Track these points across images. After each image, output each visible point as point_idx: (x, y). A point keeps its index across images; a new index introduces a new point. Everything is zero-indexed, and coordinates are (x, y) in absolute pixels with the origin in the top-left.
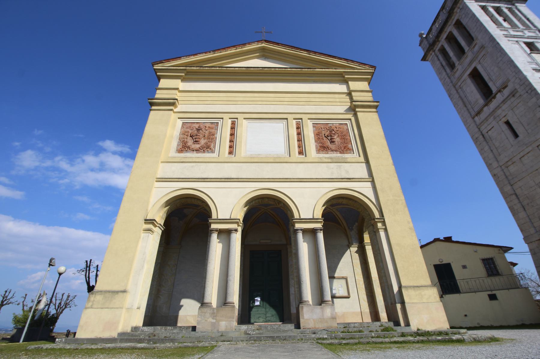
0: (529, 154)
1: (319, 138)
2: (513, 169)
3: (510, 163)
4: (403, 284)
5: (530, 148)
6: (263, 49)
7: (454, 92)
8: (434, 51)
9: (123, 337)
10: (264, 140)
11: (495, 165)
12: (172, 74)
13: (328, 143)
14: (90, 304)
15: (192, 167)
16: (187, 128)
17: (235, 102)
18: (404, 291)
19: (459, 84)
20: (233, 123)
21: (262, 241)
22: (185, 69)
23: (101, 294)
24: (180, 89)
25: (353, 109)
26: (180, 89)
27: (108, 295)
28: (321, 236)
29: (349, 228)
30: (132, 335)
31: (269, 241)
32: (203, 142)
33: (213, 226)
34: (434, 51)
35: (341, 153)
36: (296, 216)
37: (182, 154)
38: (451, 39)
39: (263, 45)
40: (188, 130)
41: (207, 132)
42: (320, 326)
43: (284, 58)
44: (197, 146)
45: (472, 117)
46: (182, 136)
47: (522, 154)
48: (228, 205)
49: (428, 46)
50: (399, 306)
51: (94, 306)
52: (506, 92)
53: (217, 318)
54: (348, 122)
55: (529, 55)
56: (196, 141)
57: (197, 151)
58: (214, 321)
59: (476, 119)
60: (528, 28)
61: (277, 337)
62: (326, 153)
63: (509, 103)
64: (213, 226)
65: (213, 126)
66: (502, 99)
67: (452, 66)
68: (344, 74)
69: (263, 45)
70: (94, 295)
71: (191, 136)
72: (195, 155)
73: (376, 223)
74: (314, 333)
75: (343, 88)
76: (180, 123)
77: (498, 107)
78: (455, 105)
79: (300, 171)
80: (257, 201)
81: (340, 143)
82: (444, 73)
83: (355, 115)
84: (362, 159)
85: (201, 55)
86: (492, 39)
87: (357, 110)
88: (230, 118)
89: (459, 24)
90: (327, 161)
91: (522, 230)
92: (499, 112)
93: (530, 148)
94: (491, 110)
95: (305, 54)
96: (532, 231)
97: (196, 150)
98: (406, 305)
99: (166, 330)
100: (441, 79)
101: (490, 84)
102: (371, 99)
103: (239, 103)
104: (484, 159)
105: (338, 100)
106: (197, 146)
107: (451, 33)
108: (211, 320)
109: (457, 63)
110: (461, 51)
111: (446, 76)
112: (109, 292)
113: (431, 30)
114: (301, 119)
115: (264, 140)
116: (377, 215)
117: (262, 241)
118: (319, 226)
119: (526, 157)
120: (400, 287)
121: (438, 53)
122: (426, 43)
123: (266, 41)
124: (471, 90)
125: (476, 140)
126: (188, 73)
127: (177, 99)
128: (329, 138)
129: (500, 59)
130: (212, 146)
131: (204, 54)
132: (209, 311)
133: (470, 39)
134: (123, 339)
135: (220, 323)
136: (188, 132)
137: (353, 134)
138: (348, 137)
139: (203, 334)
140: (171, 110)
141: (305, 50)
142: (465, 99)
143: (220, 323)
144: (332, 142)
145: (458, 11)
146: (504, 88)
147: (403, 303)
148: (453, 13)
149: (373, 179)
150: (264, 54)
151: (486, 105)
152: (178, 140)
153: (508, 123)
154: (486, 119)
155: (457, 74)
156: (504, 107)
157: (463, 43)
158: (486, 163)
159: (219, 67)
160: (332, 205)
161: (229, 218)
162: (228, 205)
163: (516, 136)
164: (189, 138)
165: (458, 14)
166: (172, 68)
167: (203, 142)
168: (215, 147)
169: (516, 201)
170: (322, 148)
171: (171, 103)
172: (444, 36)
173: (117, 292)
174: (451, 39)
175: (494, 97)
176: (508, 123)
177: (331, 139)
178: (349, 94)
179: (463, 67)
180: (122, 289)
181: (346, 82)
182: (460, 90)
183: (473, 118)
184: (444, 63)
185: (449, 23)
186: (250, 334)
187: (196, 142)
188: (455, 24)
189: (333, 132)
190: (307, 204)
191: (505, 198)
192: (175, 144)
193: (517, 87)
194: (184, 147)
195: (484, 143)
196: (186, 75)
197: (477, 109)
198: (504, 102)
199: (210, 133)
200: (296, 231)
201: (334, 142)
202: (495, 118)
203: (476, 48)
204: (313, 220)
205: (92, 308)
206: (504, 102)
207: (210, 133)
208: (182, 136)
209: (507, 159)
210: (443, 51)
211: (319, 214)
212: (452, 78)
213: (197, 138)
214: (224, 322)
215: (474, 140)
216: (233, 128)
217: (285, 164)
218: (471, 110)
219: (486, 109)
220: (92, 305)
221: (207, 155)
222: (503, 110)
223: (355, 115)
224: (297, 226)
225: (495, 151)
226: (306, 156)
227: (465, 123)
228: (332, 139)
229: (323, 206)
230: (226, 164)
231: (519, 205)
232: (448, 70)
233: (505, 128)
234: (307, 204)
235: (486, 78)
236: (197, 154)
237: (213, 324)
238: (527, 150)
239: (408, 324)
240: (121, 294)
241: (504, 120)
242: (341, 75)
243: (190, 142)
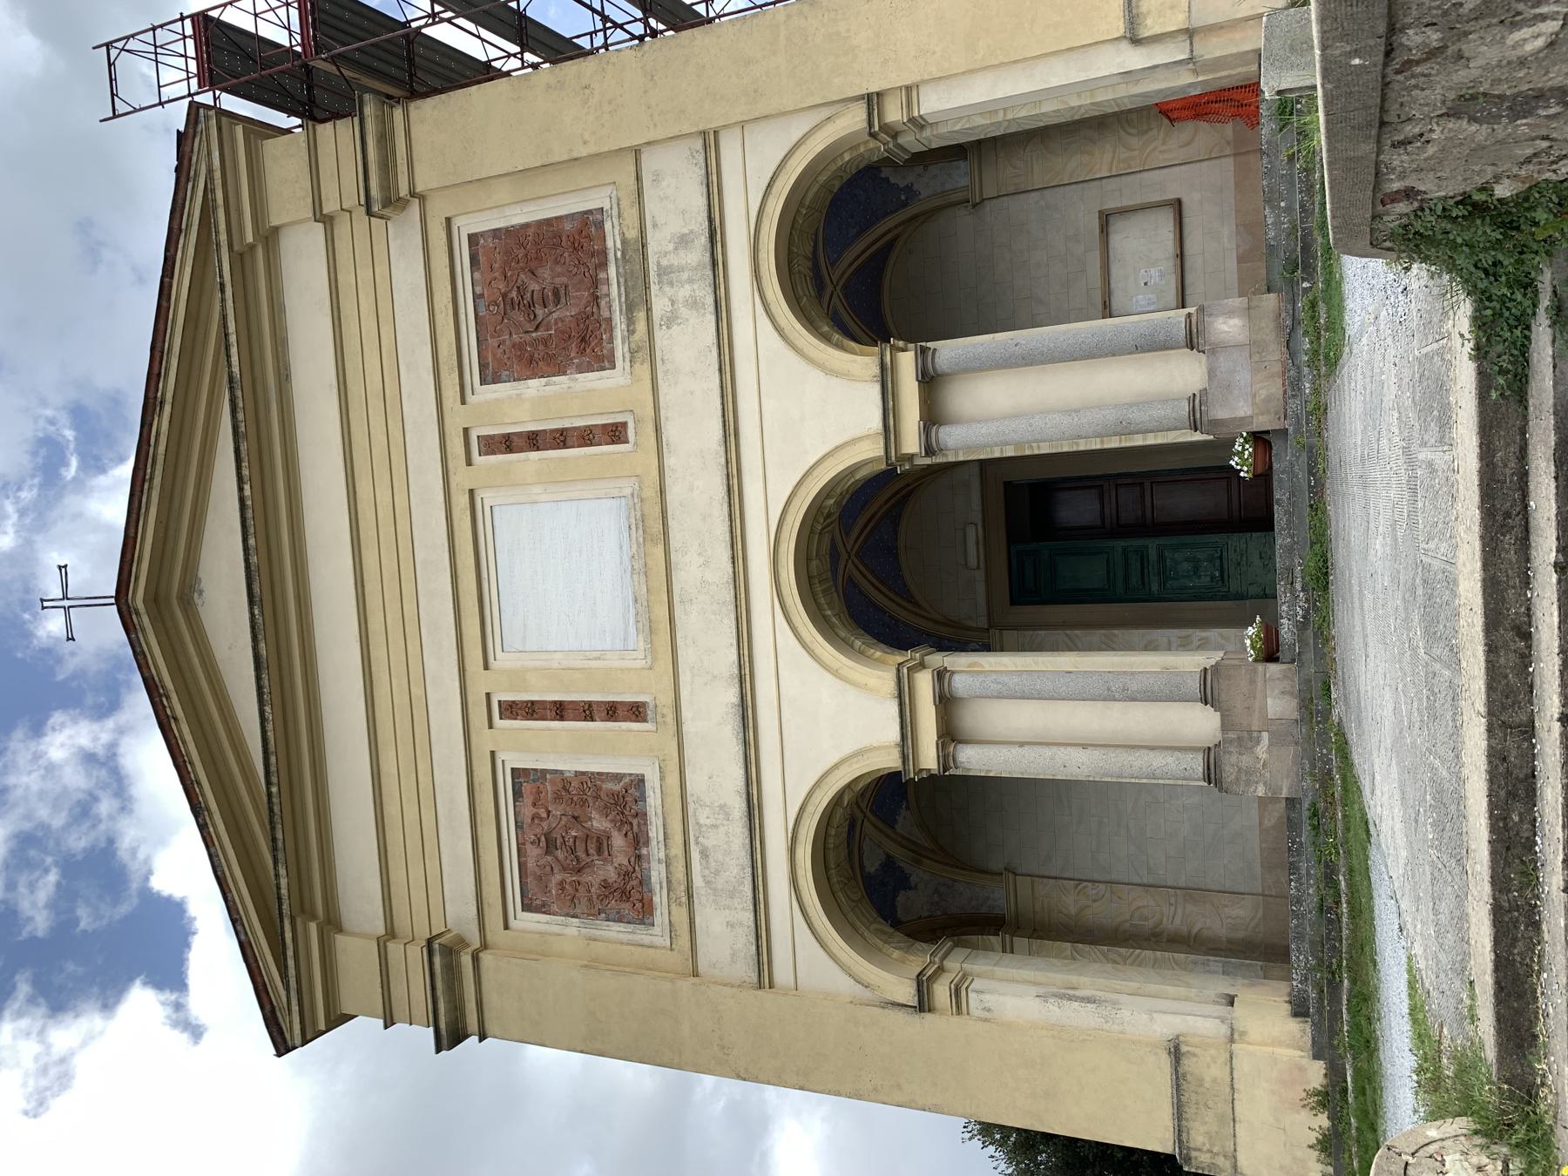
9: (1321, 1049)
10: (563, 577)
13: (565, 313)
14: (1220, 1161)
15: (704, 854)
16: (546, 890)
17: (417, 710)
20: (511, 710)
21: (973, 561)
24: (390, 945)
29: (905, 205)
31: (971, 534)
32: (599, 823)
33: (929, 759)
35: (603, 265)
42: (1277, 356)
44: (618, 841)
46: (582, 907)
48: (841, 715)
53: (1255, 728)
57: (638, 840)
58: (1265, 735)
62: (611, 329)
64: (929, 759)
65: (527, 788)
72: (656, 851)
80: (818, 588)
81: (559, 269)
90: (641, 326)
105: (365, 274)
106: (618, 841)
108: (1262, 751)
115: (563, 577)
117: (973, 561)
127: (430, 942)
132: (1234, 759)
136: (561, 884)
138: (530, 232)
140: (476, 959)
159: (273, 829)
160: (819, 285)
162: (841, 715)
164: (586, 878)
166: (292, 971)
167: (599, 823)
168: (617, 777)
170: (585, 345)
180: (1165, 1062)
186: (1307, 611)
187: (602, 844)
189: (514, 294)
190: (822, 411)
194: (628, 897)
196: (314, 917)
199: (558, 798)
204: (887, 381)
207: (558, 798)
208: (582, 907)
211: (862, 363)
216: (531, 710)
221: (653, 801)
228: (547, 296)
234: (822, 411)
236: (654, 843)
242: (241, 259)
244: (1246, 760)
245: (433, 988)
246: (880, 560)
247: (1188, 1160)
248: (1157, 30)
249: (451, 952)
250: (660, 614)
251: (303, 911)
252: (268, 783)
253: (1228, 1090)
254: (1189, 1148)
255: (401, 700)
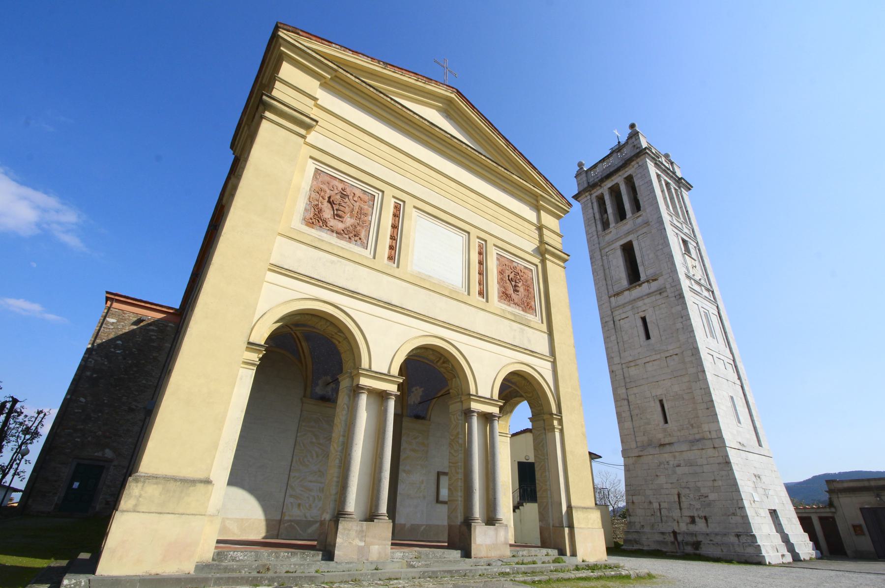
0: (655, 363)
1: (502, 279)
2: (633, 371)
3: (632, 364)
4: (573, 504)
5: (658, 356)
6: (449, 101)
7: (597, 254)
8: (591, 195)
11: (617, 360)
12: (312, 64)
15: (333, 262)
18: (576, 515)
19: (607, 250)
20: (397, 207)
22: (336, 71)
23: (156, 484)
25: (542, 251)
26: (318, 102)
27: (172, 485)
28: (391, 404)
30: (218, 568)
34: (591, 195)
35: (523, 310)
36: (365, 364)
37: (313, 230)
38: (615, 191)
39: (453, 96)
40: (325, 187)
41: (357, 205)
43: (473, 132)
45: (608, 296)
46: (314, 195)
47: (648, 359)
48: (383, 348)
49: (586, 185)
50: (567, 530)
51: (142, 508)
52: (654, 286)
53: (367, 539)
54: (533, 268)
55: (683, 254)
56: (338, 215)
58: (362, 544)
59: (613, 299)
60: (686, 223)
61: (457, 571)
63: (653, 298)
66: (647, 291)
67: (606, 225)
68: (539, 198)
69: (453, 96)
70: (140, 485)
71: (329, 201)
72: (333, 239)
73: (553, 419)
74: (489, 565)
75: (531, 215)
76: (311, 167)
77: (640, 298)
78: (594, 272)
79: (480, 321)
82: (594, 228)
83: (543, 262)
84: (544, 327)
85: (365, 59)
86: (661, 222)
87: (547, 256)
88: (394, 197)
89: (629, 180)
91: (622, 442)
92: (640, 303)
93: (658, 356)
94: (632, 298)
95: (502, 143)
96: (633, 445)
97: (337, 233)
98: (576, 530)
99: (277, 557)
100: (587, 233)
101: (641, 269)
102: (559, 246)
103: (408, 175)
104: (607, 349)
106: (340, 226)
107: (617, 185)
109: (612, 225)
110: (621, 215)
111: (595, 233)
112: (175, 479)
113: (595, 166)
114: (404, 202)
115: (437, 253)
116: (554, 411)
118: (393, 388)
119: (650, 364)
120: (570, 507)
121: (594, 200)
122: (585, 179)
123: (458, 92)
124: (618, 263)
125: (604, 324)
126: (337, 78)
128: (513, 283)
129: (660, 247)
130: (363, 234)
131: (369, 60)
132: (355, 528)
133: (637, 206)
134: (222, 578)
135: (372, 547)
137: (537, 288)
139: (348, 566)
140: (304, 137)
141: (504, 137)
142: (607, 271)
143: (372, 547)
144: (516, 291)
145: (636, 166)
146: (653, 280)
147: (571, 527)
148: (629, 164)
149: (555, 359)
150: (449, 110)
151: (628, 289)
152: (306, 200)
153: (644, 320)
154: (624, 305)
155: (608, 238)
156: (647, 301)
157: (627, 206)
158: (608, 355)
160: (297, 325)
161: (386, 372)
163: (648, 337)
165: (633, 169)
167: (349, 221)
169: (626, 408)
171: (304, 124)
172: (609, 184)
173: (193, 482)
174: (615, 191)
175: (640, 285)
176: (644, 320)
177: (516, 286)
178: (540, 228)
179: (619, 233)
181: (537, 209)
182: (605, 258)
183: (610, 297)
184: (597, 216)
185: (620, 173)
187: (337, 216)
188: (626, 178)
191: (616, 401)
192: (300, 206)
193: (668, 286)
195: (613, 331)
197: (617, 289)
198: (649, 295)
200: (357, 390)
201: (518, 291)
202: (633, 308)
203: (640, 220)
205: (135, 511)
206: (649, 295)
209: (630, 359)
210: (601, 200)
212: (601, 238)
213: (338, 208)
214: (377, 547)
215: (602, 323)
217: (463, 305)
218: (610, 287)
219: (627, 293)
220: (136, 505)
222: (645, 304)
223: (543, 262)
224: (364, 381)
225: (621, 344)
226: (398, 267)
227: (599, 299)
229: (276, 322)
230: (385, 276)
231: (628, 413)
232: (600, 227)
233: (640, 323)
234: (483, 375)
235: (639, 260)
237: (360, 549)
238: (655, 357)
239: (574, 554)
240: (201, 487)
241: (642, 314)
242: (536, 197)
243: (327, 213)
244: (353, 533)
245: (295, 110)
246: (430, 378)
247: (137, 481)
248: (784, 550)
249: (308, 128)
250: (421, 283)
251: (336, 76)
252: (392, 99)
253: (181, 511)
254: (144, 482)
255: (406, 167)
